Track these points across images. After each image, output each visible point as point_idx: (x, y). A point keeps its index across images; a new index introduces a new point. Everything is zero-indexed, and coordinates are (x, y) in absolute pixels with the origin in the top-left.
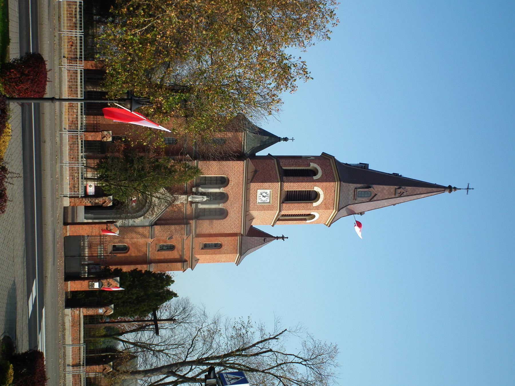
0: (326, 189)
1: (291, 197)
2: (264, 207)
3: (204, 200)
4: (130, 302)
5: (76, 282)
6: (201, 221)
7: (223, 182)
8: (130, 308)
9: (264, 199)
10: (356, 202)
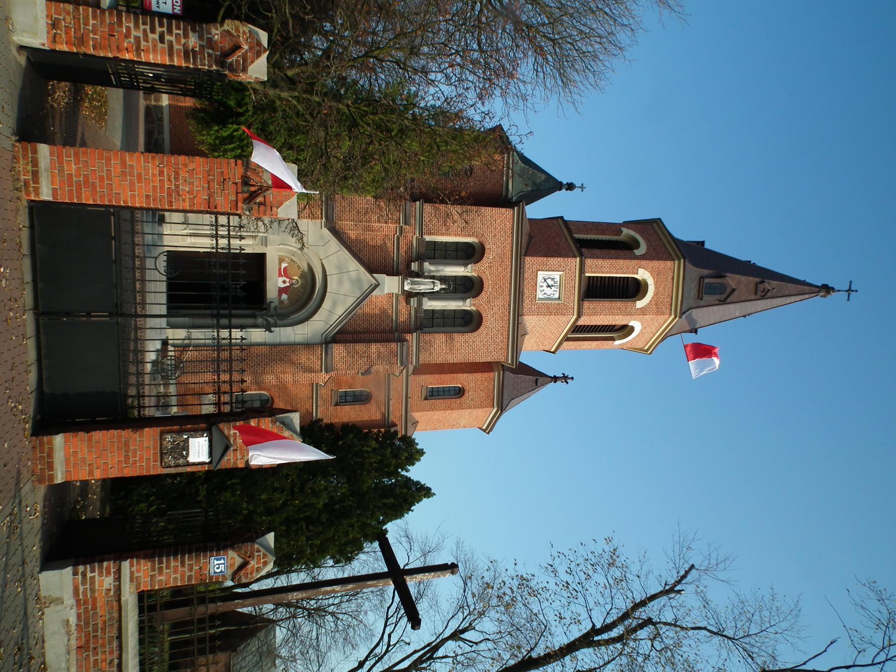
0: (658, 275)
1: (596, 290)
2: (550, 309)
3: (437, 289)
4: (309, 520)
5: (97, 435)
6: (427, 337)
7: (470, 253)
8: (308, 539)
9: (549, 291)
10: (702, 303)
